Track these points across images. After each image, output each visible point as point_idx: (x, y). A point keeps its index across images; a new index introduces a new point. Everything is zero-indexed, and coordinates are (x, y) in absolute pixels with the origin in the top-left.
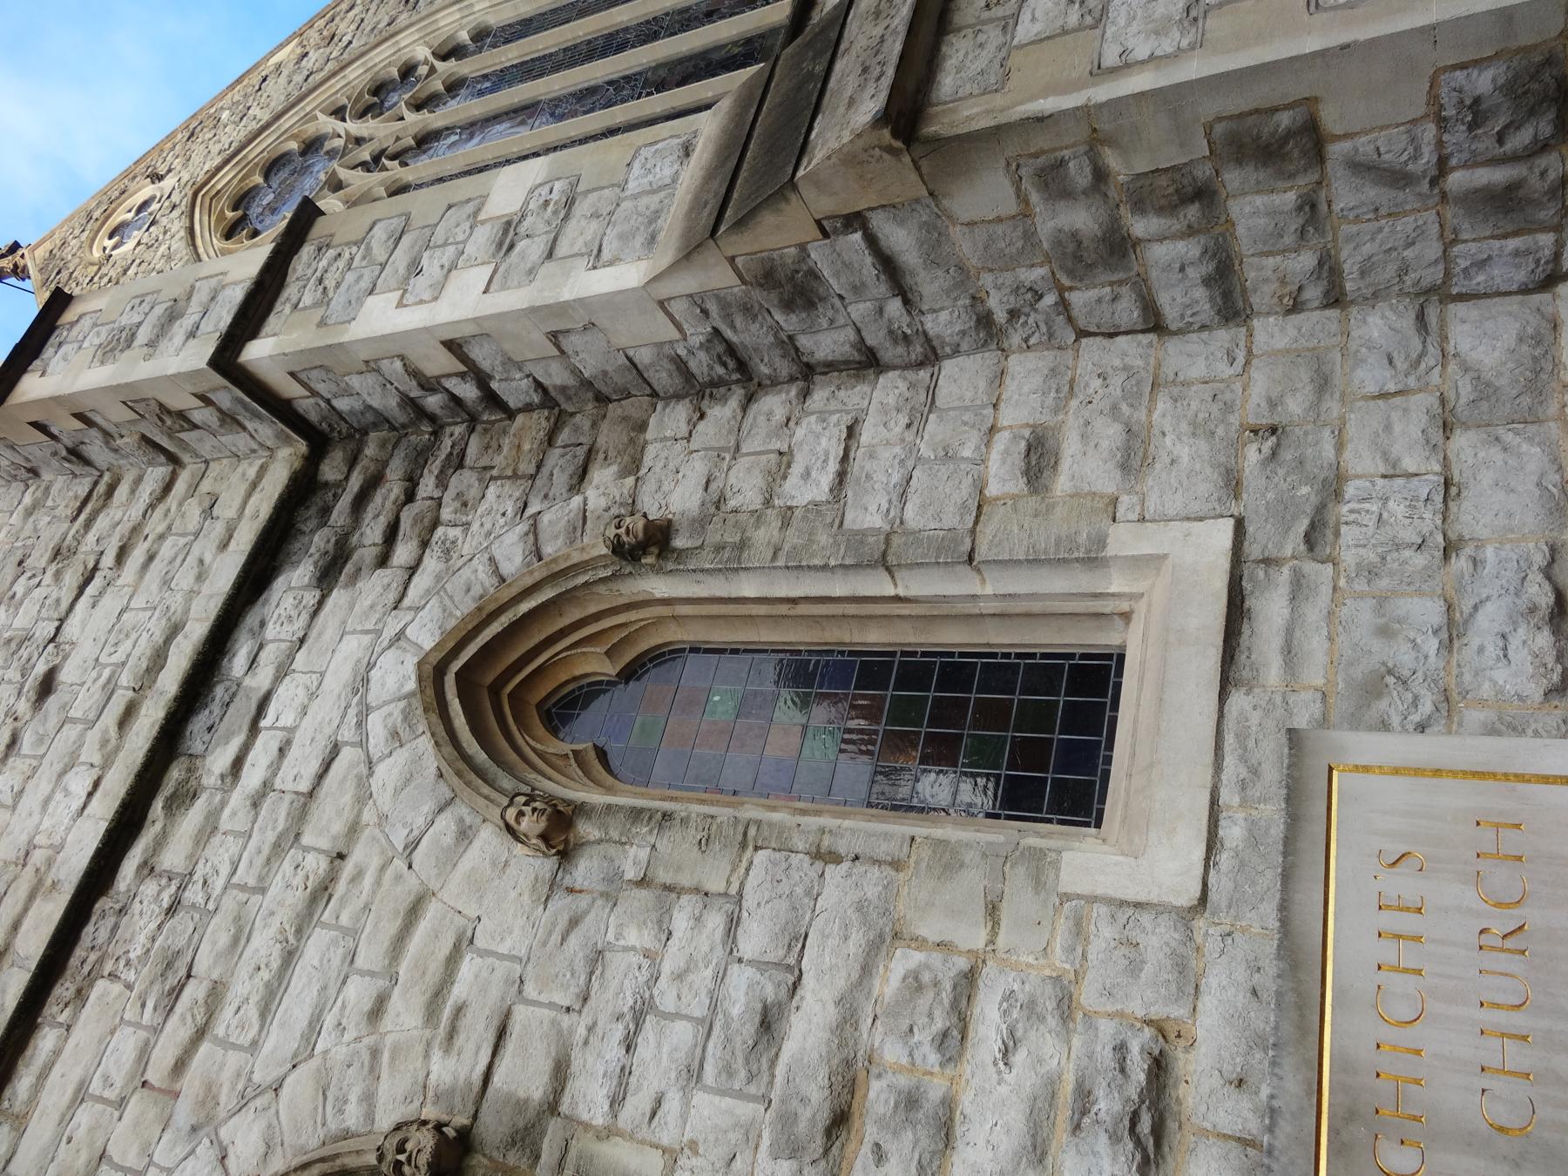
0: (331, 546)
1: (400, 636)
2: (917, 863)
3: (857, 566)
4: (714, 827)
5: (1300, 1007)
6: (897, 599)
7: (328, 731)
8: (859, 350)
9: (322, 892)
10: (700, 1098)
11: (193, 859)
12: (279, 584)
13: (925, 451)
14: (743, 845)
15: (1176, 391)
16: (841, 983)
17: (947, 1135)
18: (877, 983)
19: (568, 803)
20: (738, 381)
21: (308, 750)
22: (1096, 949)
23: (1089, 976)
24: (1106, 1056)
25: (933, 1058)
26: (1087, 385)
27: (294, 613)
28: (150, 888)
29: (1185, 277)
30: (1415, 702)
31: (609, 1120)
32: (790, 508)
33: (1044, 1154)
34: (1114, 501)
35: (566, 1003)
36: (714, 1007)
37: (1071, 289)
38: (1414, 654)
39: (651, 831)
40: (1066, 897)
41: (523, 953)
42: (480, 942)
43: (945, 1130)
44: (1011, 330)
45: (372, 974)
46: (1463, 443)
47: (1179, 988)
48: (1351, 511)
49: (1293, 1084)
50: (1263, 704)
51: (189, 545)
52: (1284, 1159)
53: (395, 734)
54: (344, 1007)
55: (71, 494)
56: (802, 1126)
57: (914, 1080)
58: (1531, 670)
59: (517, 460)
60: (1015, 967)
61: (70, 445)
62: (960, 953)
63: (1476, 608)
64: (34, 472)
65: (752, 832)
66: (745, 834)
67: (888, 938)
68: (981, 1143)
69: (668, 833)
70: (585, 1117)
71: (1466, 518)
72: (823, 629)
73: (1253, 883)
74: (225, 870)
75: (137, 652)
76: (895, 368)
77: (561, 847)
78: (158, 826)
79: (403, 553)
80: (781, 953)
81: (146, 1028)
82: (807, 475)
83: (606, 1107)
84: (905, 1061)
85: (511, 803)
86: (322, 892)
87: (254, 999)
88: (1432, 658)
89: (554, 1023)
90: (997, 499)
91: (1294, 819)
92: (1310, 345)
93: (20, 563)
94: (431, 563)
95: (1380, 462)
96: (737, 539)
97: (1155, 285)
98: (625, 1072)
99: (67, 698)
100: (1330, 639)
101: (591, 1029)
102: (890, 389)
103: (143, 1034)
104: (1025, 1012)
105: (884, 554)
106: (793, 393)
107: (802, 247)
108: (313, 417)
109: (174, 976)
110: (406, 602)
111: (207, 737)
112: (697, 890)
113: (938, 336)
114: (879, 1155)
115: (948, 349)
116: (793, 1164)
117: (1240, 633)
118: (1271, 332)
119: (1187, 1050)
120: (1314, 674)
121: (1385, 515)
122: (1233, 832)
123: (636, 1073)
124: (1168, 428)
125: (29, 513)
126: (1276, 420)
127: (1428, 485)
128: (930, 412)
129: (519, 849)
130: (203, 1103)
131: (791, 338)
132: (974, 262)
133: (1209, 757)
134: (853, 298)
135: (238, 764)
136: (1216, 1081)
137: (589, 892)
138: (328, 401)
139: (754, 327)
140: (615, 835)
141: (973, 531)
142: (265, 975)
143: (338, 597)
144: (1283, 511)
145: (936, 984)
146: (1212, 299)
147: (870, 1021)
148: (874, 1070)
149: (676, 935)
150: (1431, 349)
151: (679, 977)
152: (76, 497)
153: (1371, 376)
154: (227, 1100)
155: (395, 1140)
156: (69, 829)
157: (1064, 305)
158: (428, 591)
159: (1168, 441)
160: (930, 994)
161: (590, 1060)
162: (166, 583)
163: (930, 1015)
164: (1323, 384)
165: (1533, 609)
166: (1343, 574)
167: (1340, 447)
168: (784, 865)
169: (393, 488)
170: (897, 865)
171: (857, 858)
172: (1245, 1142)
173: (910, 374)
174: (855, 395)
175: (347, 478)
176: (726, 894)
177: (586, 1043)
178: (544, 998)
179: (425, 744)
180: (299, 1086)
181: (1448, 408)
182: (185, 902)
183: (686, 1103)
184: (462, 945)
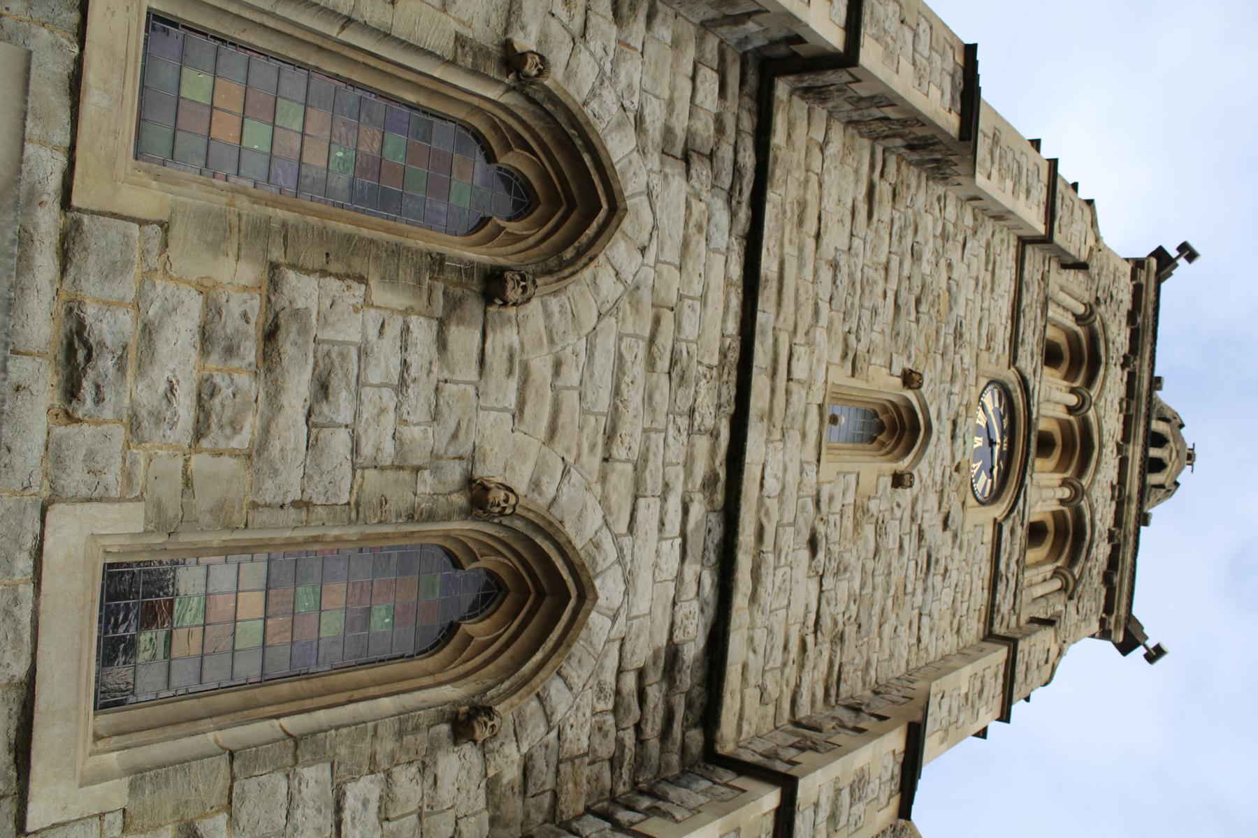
2: (241, 509)
3: (314, 733)
10: (357, 338)
14: (357, 504)
16: (281, 420)
18: (258, 424)
22: (116, 466)
23: (120, 446)
24: (108, 394)
31: (408, 319)
33: (143, 330)
35: (448, 385)
36: (358, 395)
40: (139, 499)
43: (205, 337)
45: (567, 388)
47: (60, 446)
56: (294, 328)
60: (169, 446)
65: (353, 515)
66: (358, 512)
67: (255, 454)
68: (183, 331)
69: (408, 505)
70: (422, 319)
80: (321, 435)
82: (365, 803)
84: (235, 376)
90: (218, 811)
96: (405, 739)
98: (404, 348)
101: (430, 372)
104: (162, 416)
105: (296, 746)
112: (383, 469)
114: (245, 317)
116: (296, 306)
117: (17, 730)
119: (52, 406)
130: (638, 302)
133: (43, 619)
136: (34, 388)
140: (442, 499)
141: (233, 779)
142: (627, 379)
148: (253, 368)
149: (389, 437)
151: (383, 411)
154: (625, 305)
160: (225, 420)
161: (426, 352)
163: (223, 406)
168: (329, 494)
170: (255, 506)
171: (282, 507)
172: (15, 352)
176: (363, 468)
177: (431, 363)
178: (462, 386)
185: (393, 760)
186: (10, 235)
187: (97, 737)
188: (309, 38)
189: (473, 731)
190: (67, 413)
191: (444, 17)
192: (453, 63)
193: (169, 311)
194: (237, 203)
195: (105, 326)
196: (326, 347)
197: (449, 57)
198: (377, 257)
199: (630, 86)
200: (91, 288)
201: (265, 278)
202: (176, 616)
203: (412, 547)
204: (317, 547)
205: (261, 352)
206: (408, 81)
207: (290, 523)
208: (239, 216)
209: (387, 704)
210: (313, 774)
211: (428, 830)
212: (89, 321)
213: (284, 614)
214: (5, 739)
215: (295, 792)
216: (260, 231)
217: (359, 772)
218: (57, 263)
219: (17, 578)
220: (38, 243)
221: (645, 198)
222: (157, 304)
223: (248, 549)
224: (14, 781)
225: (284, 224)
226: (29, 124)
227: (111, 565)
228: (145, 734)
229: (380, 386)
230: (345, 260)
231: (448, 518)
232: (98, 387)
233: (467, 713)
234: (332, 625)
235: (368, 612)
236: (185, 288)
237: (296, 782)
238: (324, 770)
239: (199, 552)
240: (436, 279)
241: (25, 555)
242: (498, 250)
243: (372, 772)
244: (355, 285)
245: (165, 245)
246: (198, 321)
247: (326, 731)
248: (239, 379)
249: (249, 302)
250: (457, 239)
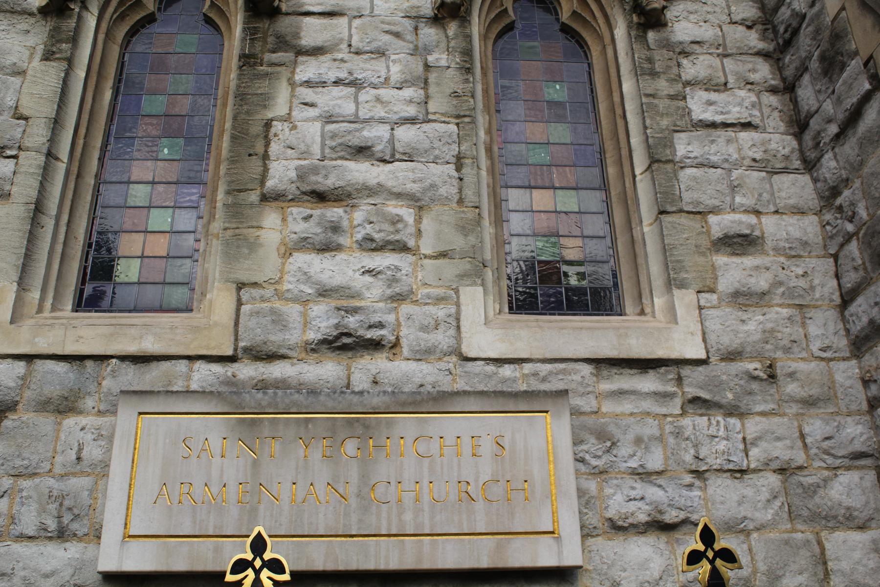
2: (463, 212)
3: (649, 147)
4: (466, 98)
5: (414, 403)
8: (806, 117)
10: (318, 125)
13: (735, 174)
14: (458, 117)
15: (798, 318)
16: (390, 184)
17: (323, 250)
18: (394, 202)
20: (778, 44)
22: (431, 309)
23: (416, 307)
24: (376, 318)
26: (797, 266)
29: (872, 307)
30: (596, 457)
31: (298, 82)
33: (324, 296)
34: (712, 291)
35: (353, 43)
36: (366, 121)
37: (858, 239)
38: (626, 455)
39: (457, 63)
40: (457, 291)
41: (376, 12)
43: (326, 248)
44: (833, 211)
46: (773, 480)
47: (418, 351)
48: (718, 422)
49: (376, 401)
50: (586, 381)
56: (313, 178)
57: (347, 229)
60: (415, 271)
63: (660, 486)
65: (467, 120)
66: (465, 116)
67: (419, 203)
68: (323, 266)
69: (458, 73)
70: (298, 70)
71: (719, 481)
72: (611, 139)
73: (480, 382)
76: (800, 144)
77: (439, 16)
80: (401, 150)
82: (710, 103)
83: (304, 79)
84: (355, 223)
88: (625, 465)
89: (341, 40)
90: (706, 222)
92: (839, 395)
95: (754, 435)
96: (658, 70)
97: (867, 292)
98: (323, 84)
100: (632, 414)
101: (342, 60)
102: (780, 142)
104: (391, 278)
105: (658, 161)
106: (773, 82)
107: (856, 53)
112: (427, 97)
113: (821, 165)
114: (307, 218)
115: (815, 174)
116: (295, 178)
117: (631, 368)
118: (847, 373)
119: (387, 358)
120: (607, 407)
121: (717, 440)
122: (507, 371)
123: (325, 90)
124: (767, 316)
126: (781, 378)
127: (738, 459)
128: (767, 172)
131: (806, 69)
132: (866, 170)
133: (549, 356)
134: (834, 100)
136: (374, 371)
137: (417, 40)
139: (808, 41)
140: (452, 44)
141: (681, 211)
144: (716, 384)
146: (863, 329)
147: (373, 202)
148: (348, 209)
149: (400, 92)
150: (840, 461)
151: (378, 99)
153: (816, 428)
157: (849, 238)
159: (761, 318)
160: (391, 229)
161: (326, 65)
163: (380, 231)
164: (809, 403)
165: (661, 512)
166: (675, 419)
167: (763, 414)
168: (450, 141)
170: (460, 201)
171: (461, 179)
172: (348, 386)
173: (796, 155)
174: (775, 122)
176: (427, 113)
177: (335, 60)
178: (353, 31)
181: (796, 471)
183: (314, 119)
185: (675, 80)
186: (260, 395)
187: (642, 313)
188: (72, 185)
189: (655, 9)
190: (392, 347)
191: (30, 72)
192: (70, 62)
193: (307, 278)
194: (215, 231)
195: (323, 325)
196: (327, 151)
197: (65, 65)
198: (248, 113)
200: (295, 336)
201: (273, 204)
202: (551, 259)
203: (495, 68)
204: (495, 148)
205: (335, 204)
206: (94, 99)
207: (474, 172)
208: (225, 229)
209: (628, 86)
210: (682, 147)
211: (738, 48)
212: (320, 337)
213: (551, 173)
214: (637, 376)
215: (696, 161)
216: (236, 211)
217: (684, 109)
218: (278, 362)
219: (518, 375)
220: (264, 376)
222: (302, 287)
223: (498, 203)
224: (668, 368)
225: (228, 193)
226: (175, 389)
227: (511, 308)
228: (641, 279)
229: (357, 103)
230: (252, 139)
231: (468, 38)
232: (370, 327)
233: (639, 15)
234: (560, 132)
235: (551, 104)
236: (288, 267)
237: (688, 161)
238: (680, 138)
239: (500, 242)
240: (262, 60)
241: (501, 370)
242: (232, 5)
243: (685, 98)
244: (273, 130)
245: (255, 284)
246: (313, 255)
247: (647, 137)
248: (358, 218)
249: (295, 216)
250: (226, 44)
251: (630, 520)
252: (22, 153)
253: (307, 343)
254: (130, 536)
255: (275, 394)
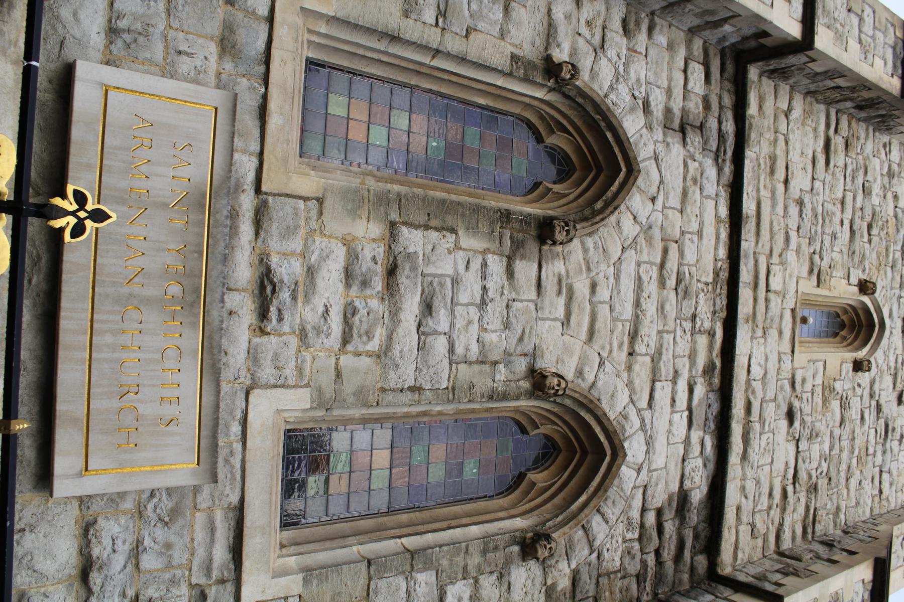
0: (687, 516)
1: (639, 471)
3: (425, 549)
5: (212, 347)
6: (400, 537)
7: (656, 414)
9: (634, 336)
11: (694, 342)
12: (705, 490)
14: (453, 389)
16: (400, 330)
18: (384, 333)
19: (538, 398)
21: (662, 403)
23: (294, 350)
24: (287, 316)
25: (357, 304)
27: (692, 474)
28: (707, 325)
31: (486, 257)
32: (464, 579)
35: (515, 303)
36: (452, 312)
40: (307, 386)
42: (559, 324)
43: (348, 275)
45: (601, 303)
47: (257, 351)
49: (214, 314)
51: (755, 506)
52: (218, 283)
53: (626, 418)
54: (608, 286)
55: (823, 524)
56: (407, 266)
58: (103, 534)
59: (610, 585)
60: (326, 350)
61: (834, 549)
62: (350, 352)
63: (125, 567)
64: (845, 532)
65: (451, 396)
66: (454, 394)
67: (383, 355)
68: (333, 271)
70: (496, 257)
74: (678, 339)
75: (757, 441)
78: (714, 355)
79: (651, 518)
80: (428, 340)
81: (685, 265)
84: (369, 300)
85: (564, 390)
86: (634, 336)
87: (646, 284)
88: (147, 534)
91: (214, 437)
93: (830, 479)
94: (635, 514)
96: (488, 555)
98: (484, 277)
99: (779, 412)
100: (193, 539)
101: (502, 294)
103: (685, 262)
105: (413, 558)
108: (721, 588)
109: (682, 288)
110: (641, 490)
111: (709, 401)
112: (471, 363)
114: (374, 260)
116: (408, 251)
117: (234, 538)
122: (236, 429)
125: (838, 509)
129: (554, 370)
130: (651, 238)
133: (248, 465)
135: (691, 391)
138: (717, 597)
140: (513, 384)
141: (370, 579)
142: (645, 295)
143: (675, 487)
145: (360, 336)
148: (380, 295)
149: (475, 341)
151: (470, 322)
152: (819, 522)
154: (641, 240)
155: (571, 234)
156: (752, 347)
158: (633, 498)
160: (362, 331)
162: (758, 482)
163: (361, 321)
165: (101, 568)
168: (434, 382)
169: (668, 555)
170: (383, 390)
171: (401, 391)
172: (229, 289)
175: (692, 558)
176: (457, 363)
177: (503, 287)
178: (526, 303)
179: (612, 416)
180: (615, 251)
182: (690, 321)
183: (456, 269)
184: (566, 321)
192: (510, 75)
195: (283, 270)
199: (638, 80)
221: (653, 161)
244: (448, 234)
251: (94, 540)
252: (440, 30)
253: (268, 255)
254: (107, 91)
255: (226, 226)
